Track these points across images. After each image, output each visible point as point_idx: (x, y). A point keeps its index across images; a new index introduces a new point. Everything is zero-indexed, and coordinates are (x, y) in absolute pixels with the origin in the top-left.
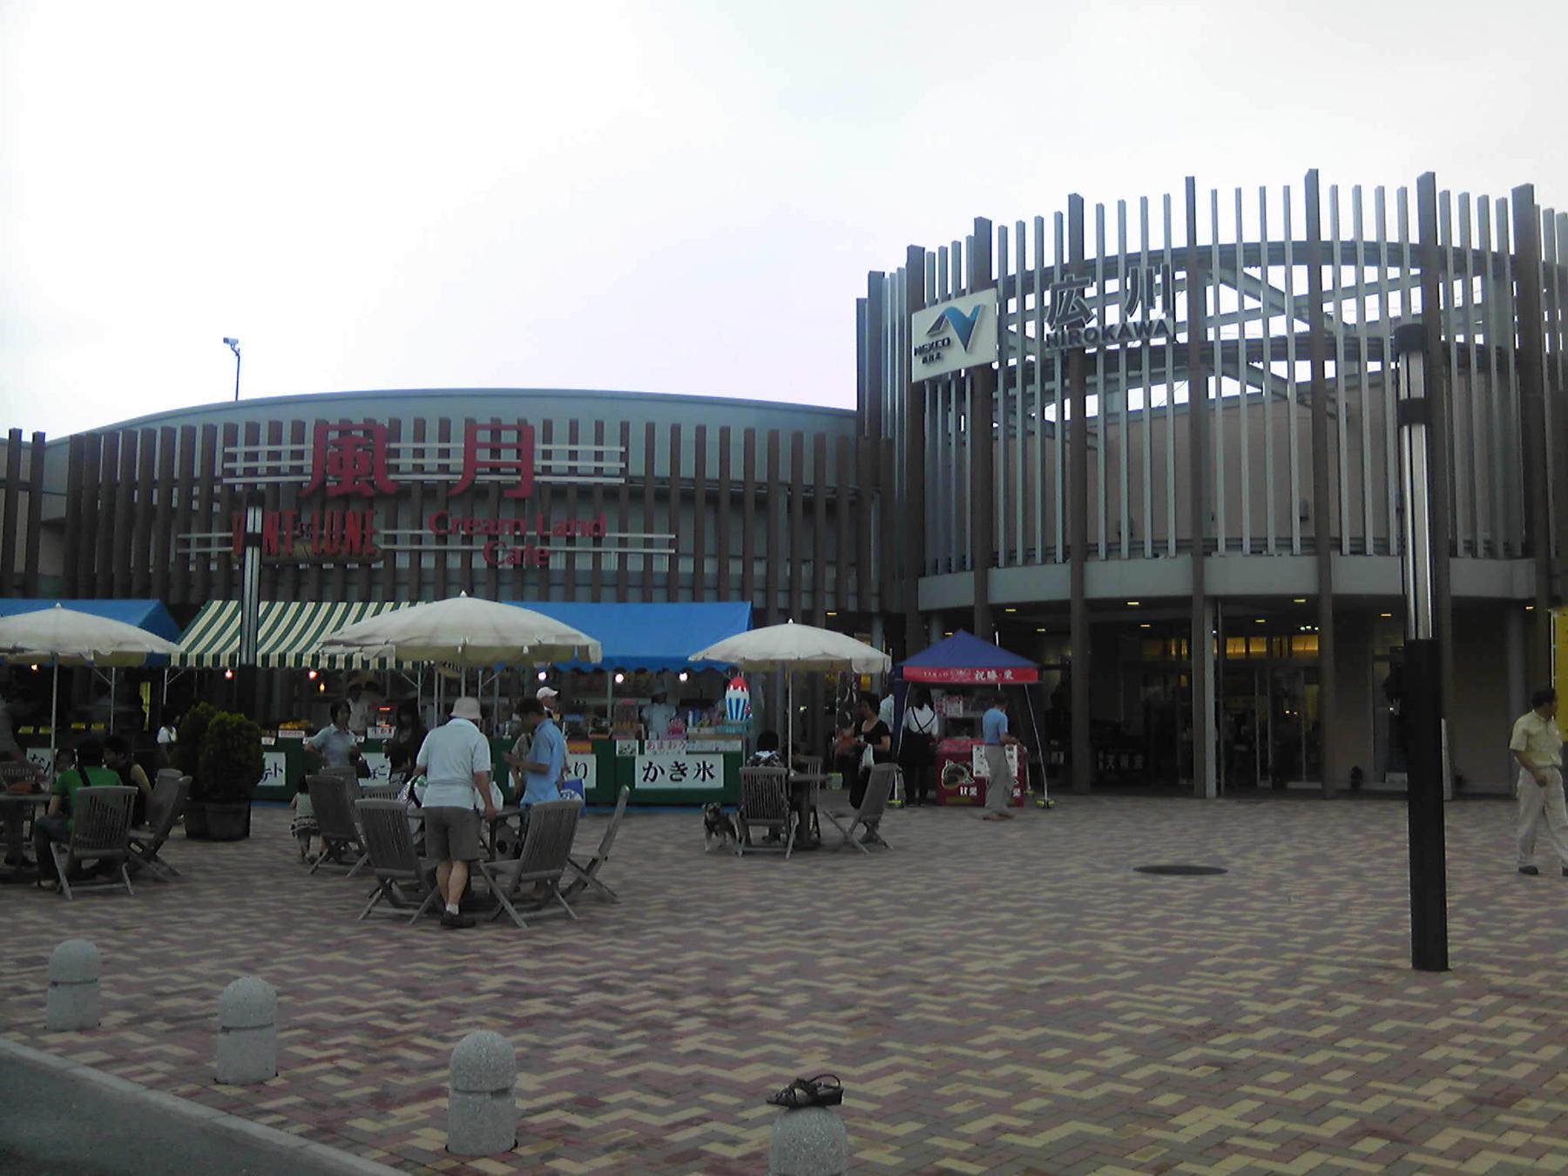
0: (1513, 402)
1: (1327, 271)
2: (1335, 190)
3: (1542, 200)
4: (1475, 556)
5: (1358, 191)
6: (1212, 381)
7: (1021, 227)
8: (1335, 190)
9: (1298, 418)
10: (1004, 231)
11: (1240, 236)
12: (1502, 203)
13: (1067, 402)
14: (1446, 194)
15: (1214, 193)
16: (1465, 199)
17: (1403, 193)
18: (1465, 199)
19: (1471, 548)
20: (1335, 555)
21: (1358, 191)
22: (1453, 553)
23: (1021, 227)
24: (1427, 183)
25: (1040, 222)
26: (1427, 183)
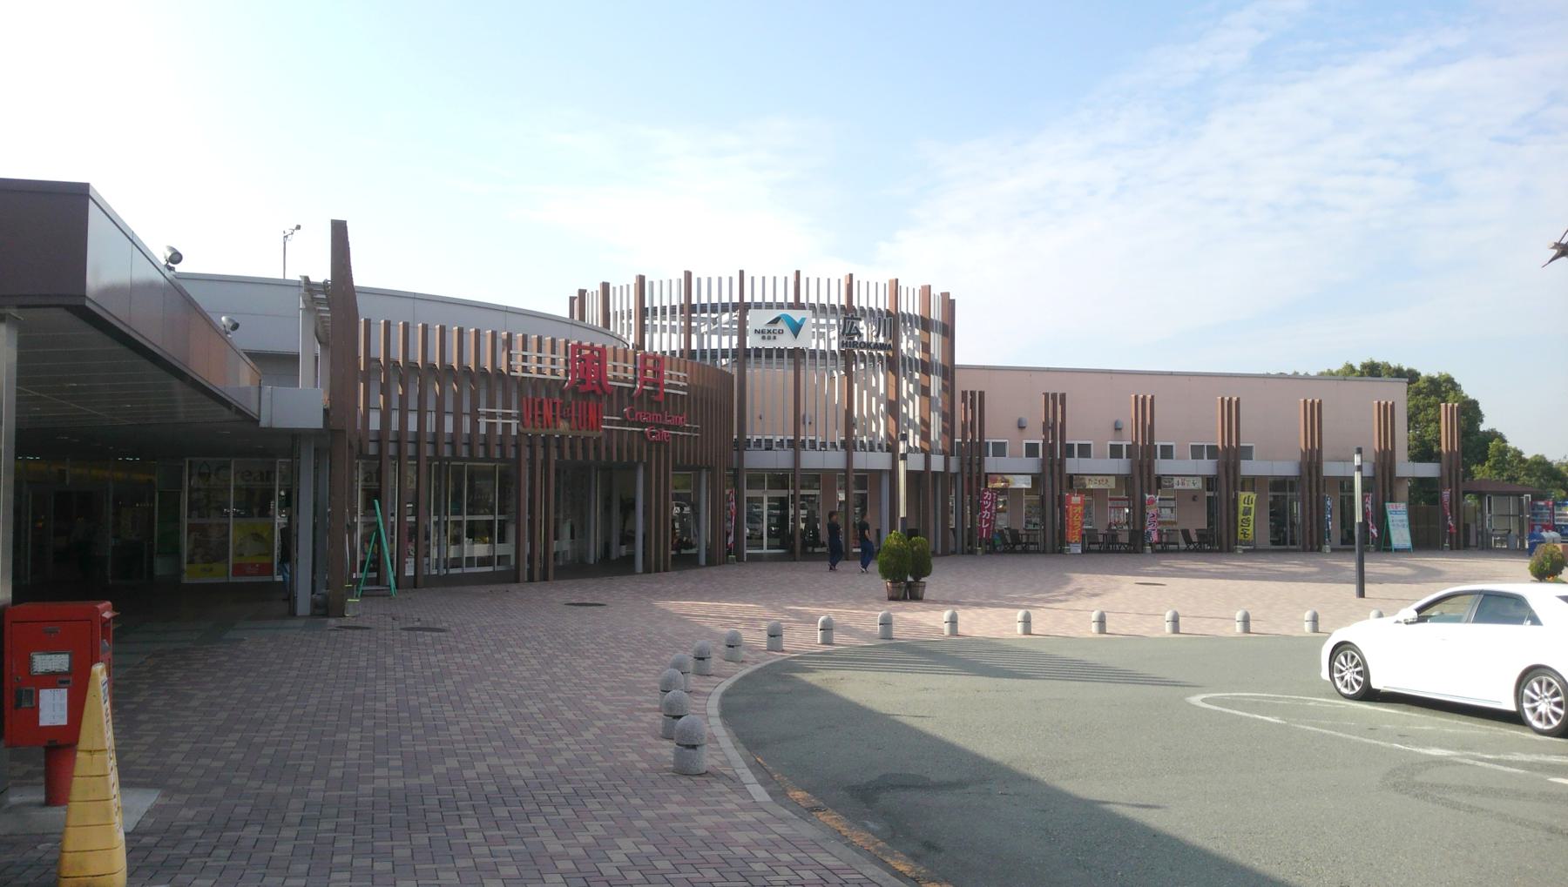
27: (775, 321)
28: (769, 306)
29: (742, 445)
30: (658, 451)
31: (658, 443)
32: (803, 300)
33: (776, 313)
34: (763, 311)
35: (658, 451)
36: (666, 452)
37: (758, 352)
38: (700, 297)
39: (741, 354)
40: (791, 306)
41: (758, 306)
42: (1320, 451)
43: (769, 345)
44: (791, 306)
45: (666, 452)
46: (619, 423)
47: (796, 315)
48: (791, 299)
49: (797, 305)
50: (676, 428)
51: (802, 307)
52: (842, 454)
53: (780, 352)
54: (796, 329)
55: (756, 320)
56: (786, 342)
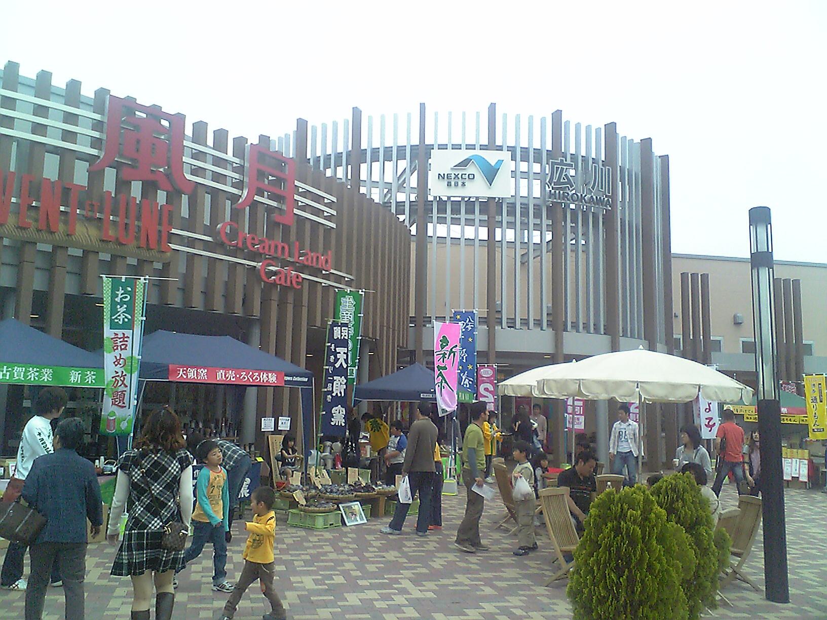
0: (601, 295)
1: (498, 231)
2: (505, 116)
3: (621, 131)
4: (578, 331)
5: (518, 117)
6: (430, 226)
7: (324, 128)
8: (505, 116)
9: (481, 254)
10: (314, 129)
11: (450, 139)
12: (598, 130)
13: (349, 167)
14: (567, 123)
15: (436, 114)
16: (578, 126)
17: (543, 120)
18: (578, 126)
19: (575, 326)
20: (498, 328)
21: (518, 117)
22: (565, 330)
23: (324, 128)
24: (557, 116)
25: (335, 124)
26: (557, 116)
27: (465, 163)
28: (457, 147)
29: (422, 321)
30: (282, 304)
31: (285, 289)
32: (499, 142)
33: (464, 154)
34: (450, 151)
35: (282, 304)
36: (297, 306)
37: (442, 204)
38: (370, 140)
39: (421, 211)
40: (483, 148)
41: (443, 147)
42: (779, 402)
43: (457, 193)
44: (483, 148)
45: (297, 306)
46: (206, 246)
47: (492, 157)
48: (484, 141)
49: (491, 146)
50: (316, 272)
51: (500, 148)
52: (548, 333)
53: (470, 205)
54: (491, 174)
55: (441, 163)
56: (477, 189)
